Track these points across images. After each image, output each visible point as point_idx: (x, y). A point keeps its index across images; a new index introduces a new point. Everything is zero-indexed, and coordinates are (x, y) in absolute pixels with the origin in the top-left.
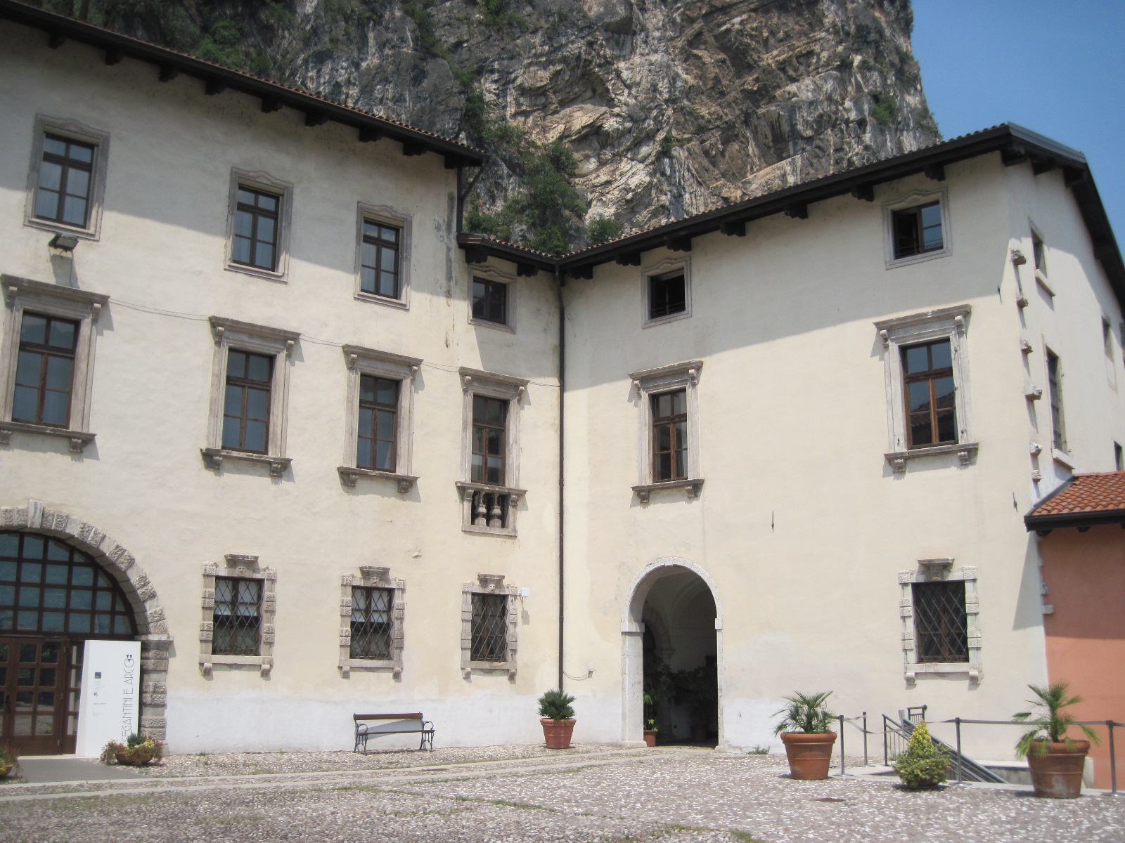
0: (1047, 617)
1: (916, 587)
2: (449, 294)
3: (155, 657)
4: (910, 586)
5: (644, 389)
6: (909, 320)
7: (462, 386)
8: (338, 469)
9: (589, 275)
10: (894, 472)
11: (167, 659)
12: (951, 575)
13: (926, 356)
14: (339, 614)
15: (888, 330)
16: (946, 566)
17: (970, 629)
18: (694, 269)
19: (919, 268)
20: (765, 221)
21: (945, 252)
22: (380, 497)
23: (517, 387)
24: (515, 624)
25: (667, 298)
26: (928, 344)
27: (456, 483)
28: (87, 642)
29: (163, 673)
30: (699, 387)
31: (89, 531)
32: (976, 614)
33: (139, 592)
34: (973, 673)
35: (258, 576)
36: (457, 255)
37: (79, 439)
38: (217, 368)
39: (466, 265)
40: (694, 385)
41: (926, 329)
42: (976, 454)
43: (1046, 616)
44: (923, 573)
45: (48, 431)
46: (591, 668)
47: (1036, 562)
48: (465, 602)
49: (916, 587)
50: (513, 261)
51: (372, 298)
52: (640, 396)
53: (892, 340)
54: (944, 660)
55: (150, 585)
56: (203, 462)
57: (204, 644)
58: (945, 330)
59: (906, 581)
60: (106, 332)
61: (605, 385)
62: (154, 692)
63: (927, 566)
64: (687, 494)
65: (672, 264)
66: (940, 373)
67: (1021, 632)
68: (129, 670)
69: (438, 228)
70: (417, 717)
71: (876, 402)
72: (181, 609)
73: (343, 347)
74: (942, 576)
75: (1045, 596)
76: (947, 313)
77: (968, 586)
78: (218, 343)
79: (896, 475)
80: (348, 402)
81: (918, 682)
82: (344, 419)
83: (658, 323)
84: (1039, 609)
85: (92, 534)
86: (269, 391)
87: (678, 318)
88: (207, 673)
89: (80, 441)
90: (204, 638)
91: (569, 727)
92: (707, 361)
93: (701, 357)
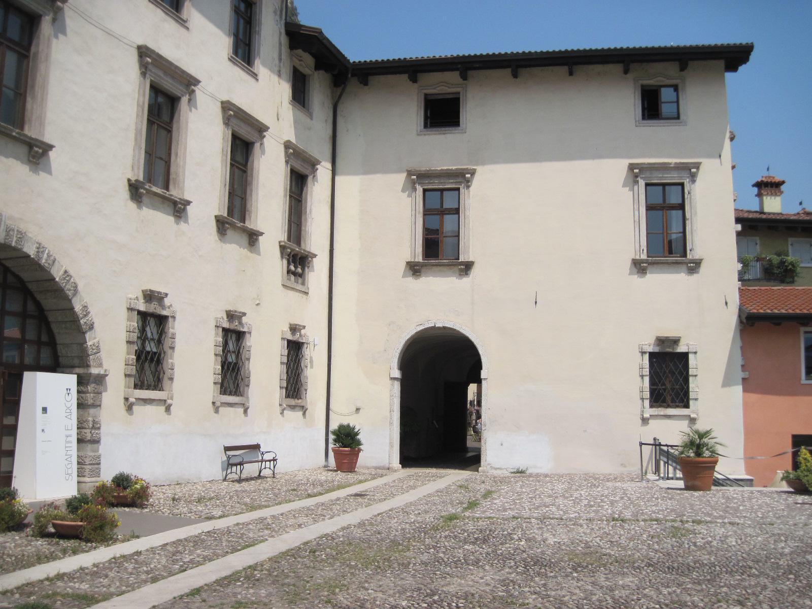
0: (744, 380)
1: (652, 355)
2: (279, 76)
3: (89, 386)
4: (648, 355)
5: (419, 184)
6: (656, 166)
7: (285, 158)
8: (216, 217)
9: (366, 83)
10: (638, 273)
11: (101, 393)
12: (679, 348)
13: (661, 191)
14: (213, 353)
15: (635, 172)
16: (676, 341)
17: (691, 385)
18: (469, 95)
19: (658, 130)
20: (535, 70)
21: (681, 123)
22: (238, 247)
23: (313, 164)
24: (306, 367)
25: (442, 114)
26: (664, 185)
27: (280, 242)
28: (27, 375)
29: (99, 408)
30: (471, 188)
31: (43, 252)
32: (696, 376)
33: (82, 322)
34: (693, 416)
35: (164, 313)
36: (285, 40)
37: (40, 148)
38: (141, 99)
39: (289, 50)
40: (468, 187)
41: (668, 174)
42: (699, 266)
43: (744, 379)
44: (658, 345)
45: (14, 134)
46: (359, 405)
47: (739, 343)
48: (283, 347)
49: (652, 355)
50: (674, 60)
51: (240, 63)
52: (415, 190)
53: (641, 178)
54: (668, 406)
55: (90, 315)
56: (128, 192)
57: (128, 379)
58: (681, 177)
59: (646, 351)
60: (61, 36)
61: (378, 176)
62: (93, 428)
63: (661, 341)
64: (458, 272)
65: (449, 88)
66: (672, 207)
67: (726, 389)
68: (68, 405)
69: (275, 12)
70: (257, 447)
71: (624, 222)
72: (111, 342)
73: (222, 103)
74: (673, 349)
75: (743, 366)
76: (685, 165)
77: (691, 356)
78: (144, 74)
79: (639, 274)
80: (223, 154)
81: (650, 421)
82: (220, 170)
83: (433, 132)
84: (740, 375)
85: (45, 255)
86: (170, 131)
87: (453, 131)
88: (130, 408)
89: (40, 151)
90: (128, 373)
91: (355, 453)
92: (480, 169)
93: (474, 165)
